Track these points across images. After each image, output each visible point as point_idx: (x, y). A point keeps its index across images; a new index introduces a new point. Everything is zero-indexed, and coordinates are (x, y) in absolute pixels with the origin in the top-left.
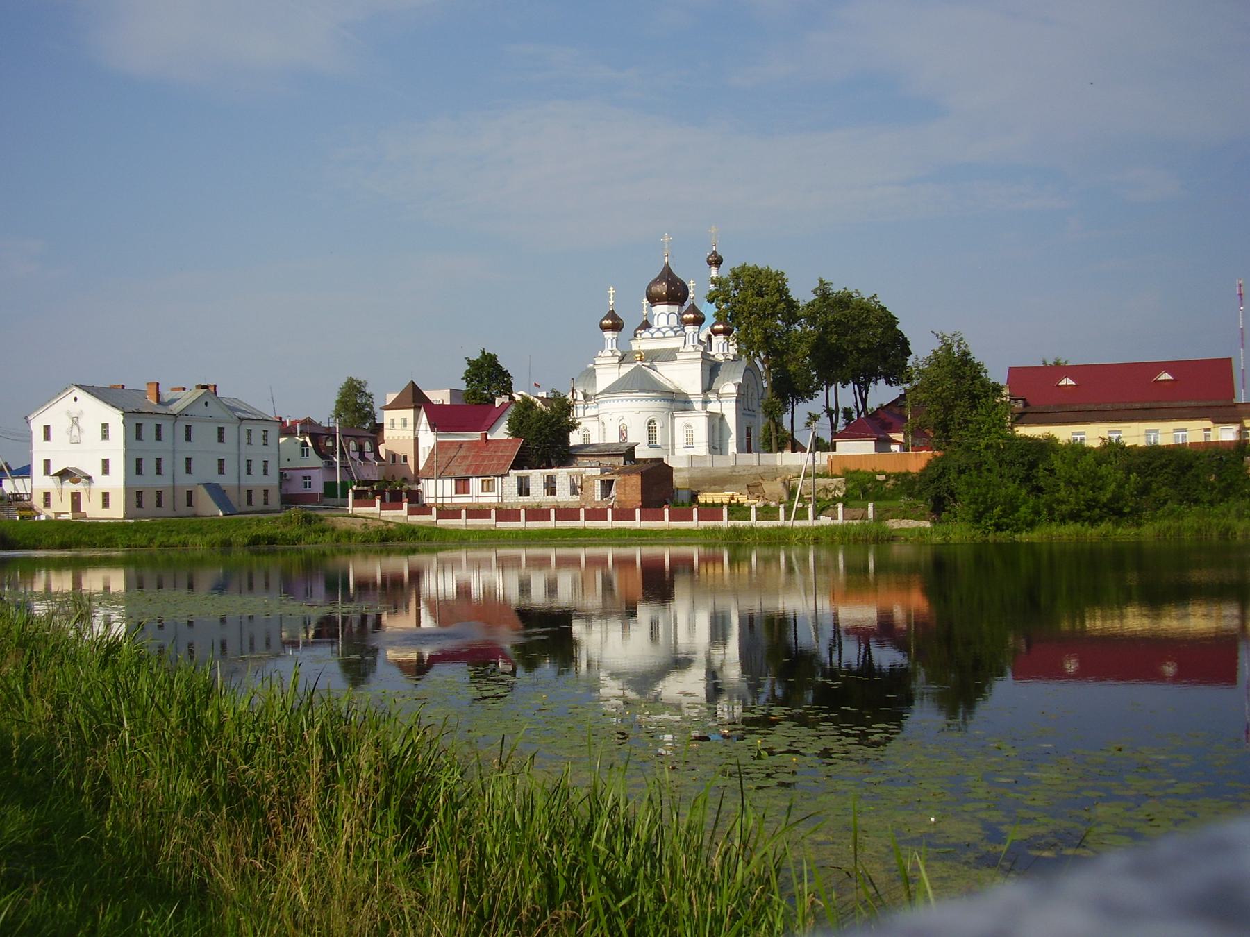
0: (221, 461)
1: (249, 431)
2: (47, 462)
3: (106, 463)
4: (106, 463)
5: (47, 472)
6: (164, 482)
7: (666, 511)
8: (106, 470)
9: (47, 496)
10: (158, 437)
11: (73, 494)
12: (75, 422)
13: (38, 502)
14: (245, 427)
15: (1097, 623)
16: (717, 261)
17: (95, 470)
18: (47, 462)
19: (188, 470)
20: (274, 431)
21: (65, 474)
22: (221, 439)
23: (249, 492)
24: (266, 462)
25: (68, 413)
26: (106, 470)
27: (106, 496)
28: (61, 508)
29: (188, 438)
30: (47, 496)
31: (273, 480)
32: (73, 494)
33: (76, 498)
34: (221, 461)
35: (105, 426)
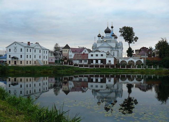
0: (40, 56)
1: (44, 51)
2: (10, 55)
3: (21, 56)
4: (21, 56)
5: (10, 57)
6: (31, 59)
7: (152, 67)
8: (21, 57)
9: (10, 61)
10: (30, 51)
11: (15, 61)
12: (15, 48)
13: (8, 62)
14: (44, 50)
15: (121, 119)
16: (112, 27)
17: (19, 57)
18: (10, 55)
19: (35, 58)
20: (48, 51)
21: (14, 58)
22: (40, 52)
23: (27, 61)
24: (30, 55)
25: (14, 47)
26: (21, 57)
27: (21, 62)
28: (12, 64)
29: (35, 52)
30: (10, 61)
31: (47, 60)
32: (15, 61)
33: (15, 62)
34: (40, 56)
35: (21, 49)
